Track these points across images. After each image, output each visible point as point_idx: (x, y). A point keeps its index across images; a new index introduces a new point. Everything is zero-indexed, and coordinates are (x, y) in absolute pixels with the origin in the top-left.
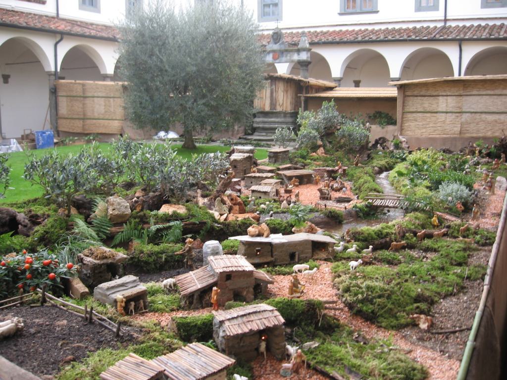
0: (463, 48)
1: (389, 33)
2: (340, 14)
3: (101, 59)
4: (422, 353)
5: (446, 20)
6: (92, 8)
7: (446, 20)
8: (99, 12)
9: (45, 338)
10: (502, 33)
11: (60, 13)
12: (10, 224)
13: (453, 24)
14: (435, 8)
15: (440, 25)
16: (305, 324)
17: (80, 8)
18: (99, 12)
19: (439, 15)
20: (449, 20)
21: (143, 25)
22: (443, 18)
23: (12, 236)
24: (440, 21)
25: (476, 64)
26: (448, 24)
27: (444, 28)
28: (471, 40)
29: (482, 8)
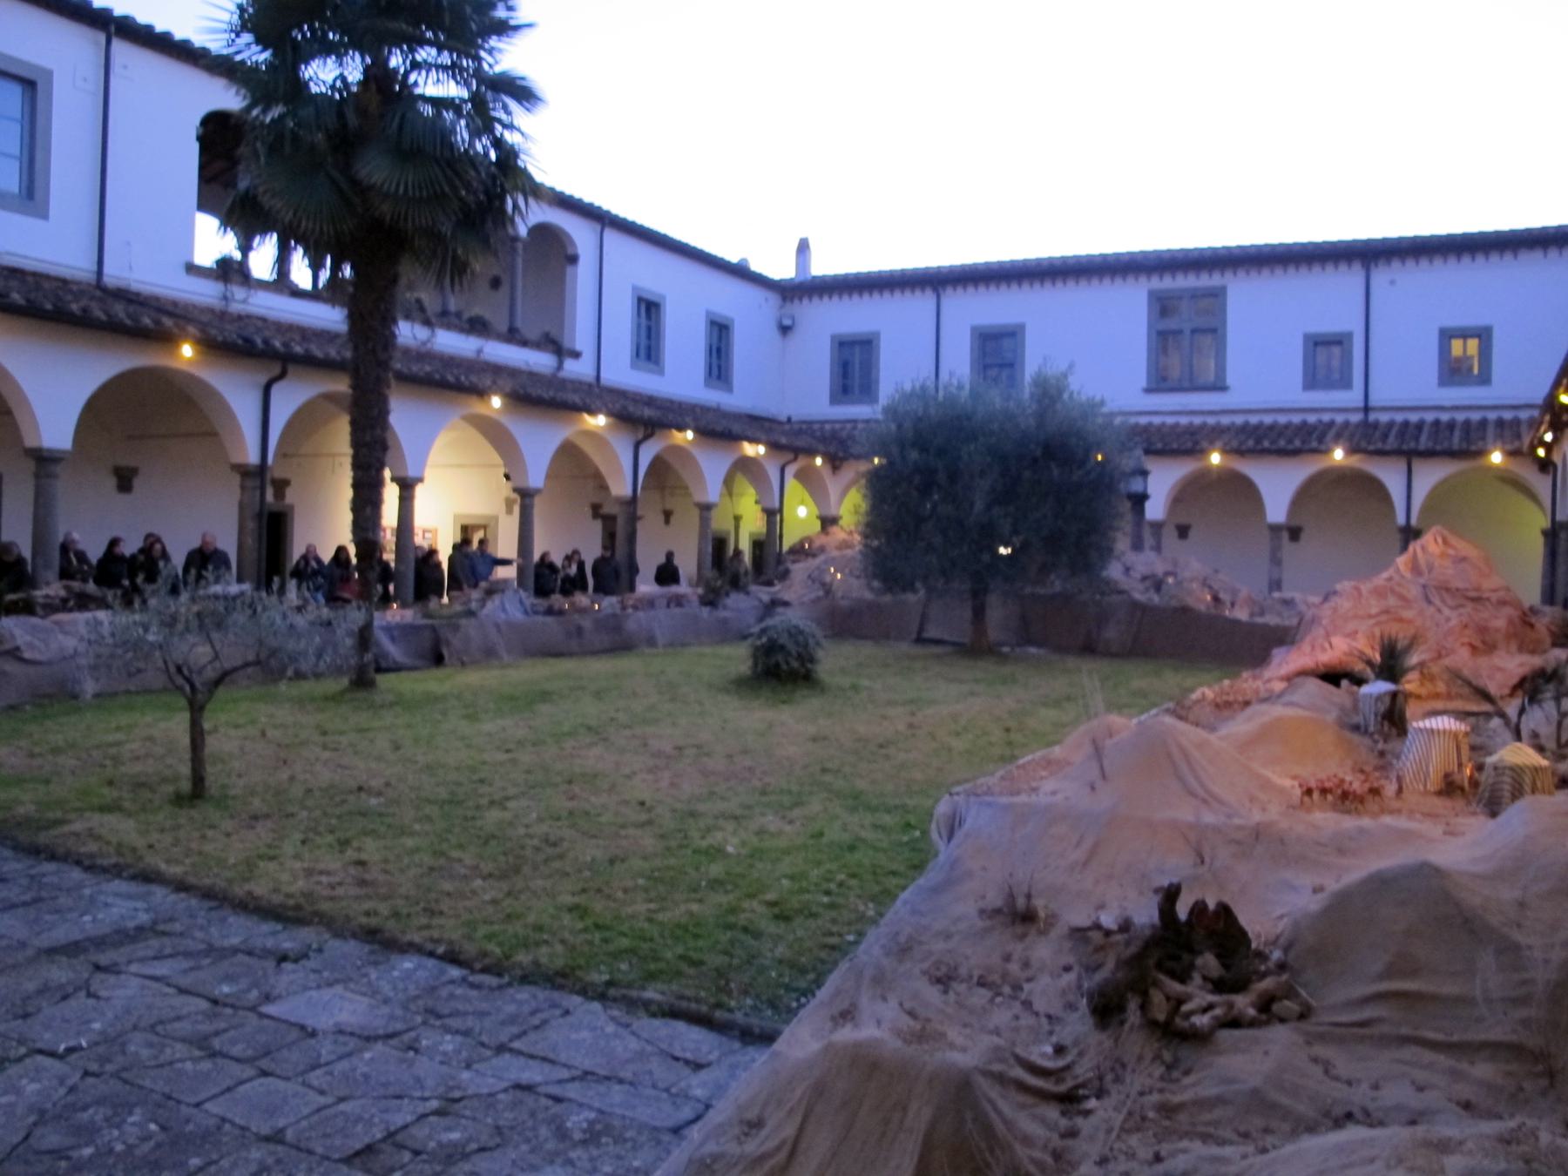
0: (1414, 468)
1: (1310, 434)
2: (1148, 390)
3: (33, 415)
4: (284, 775)
5: (1367, 409)
6: (652, 366)
7: (1367, 409)
8: (661, 372)
9: (532, 1151)
10: (1423, 438)
11: (602, 375)
12: (32, 842)
13: (1384, 418)
14: (1346, 384)
15: (1356, 418)
16: (1521, 1089)
17: (633, 366)
18: (661, 372)
19: (1353, 397)
20: (1375, 409)
21: (900, 426)
22: (1362, 404)
23: (211, 909)
24: (1355, 410)
25: (481, 393)
26: (1372, 417)
27: (1365, 424)
28: (1430, 454)
29: (877, 335)
